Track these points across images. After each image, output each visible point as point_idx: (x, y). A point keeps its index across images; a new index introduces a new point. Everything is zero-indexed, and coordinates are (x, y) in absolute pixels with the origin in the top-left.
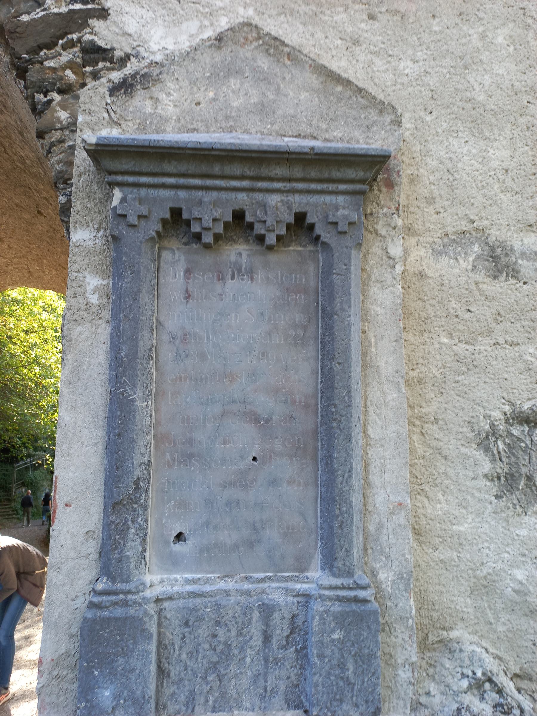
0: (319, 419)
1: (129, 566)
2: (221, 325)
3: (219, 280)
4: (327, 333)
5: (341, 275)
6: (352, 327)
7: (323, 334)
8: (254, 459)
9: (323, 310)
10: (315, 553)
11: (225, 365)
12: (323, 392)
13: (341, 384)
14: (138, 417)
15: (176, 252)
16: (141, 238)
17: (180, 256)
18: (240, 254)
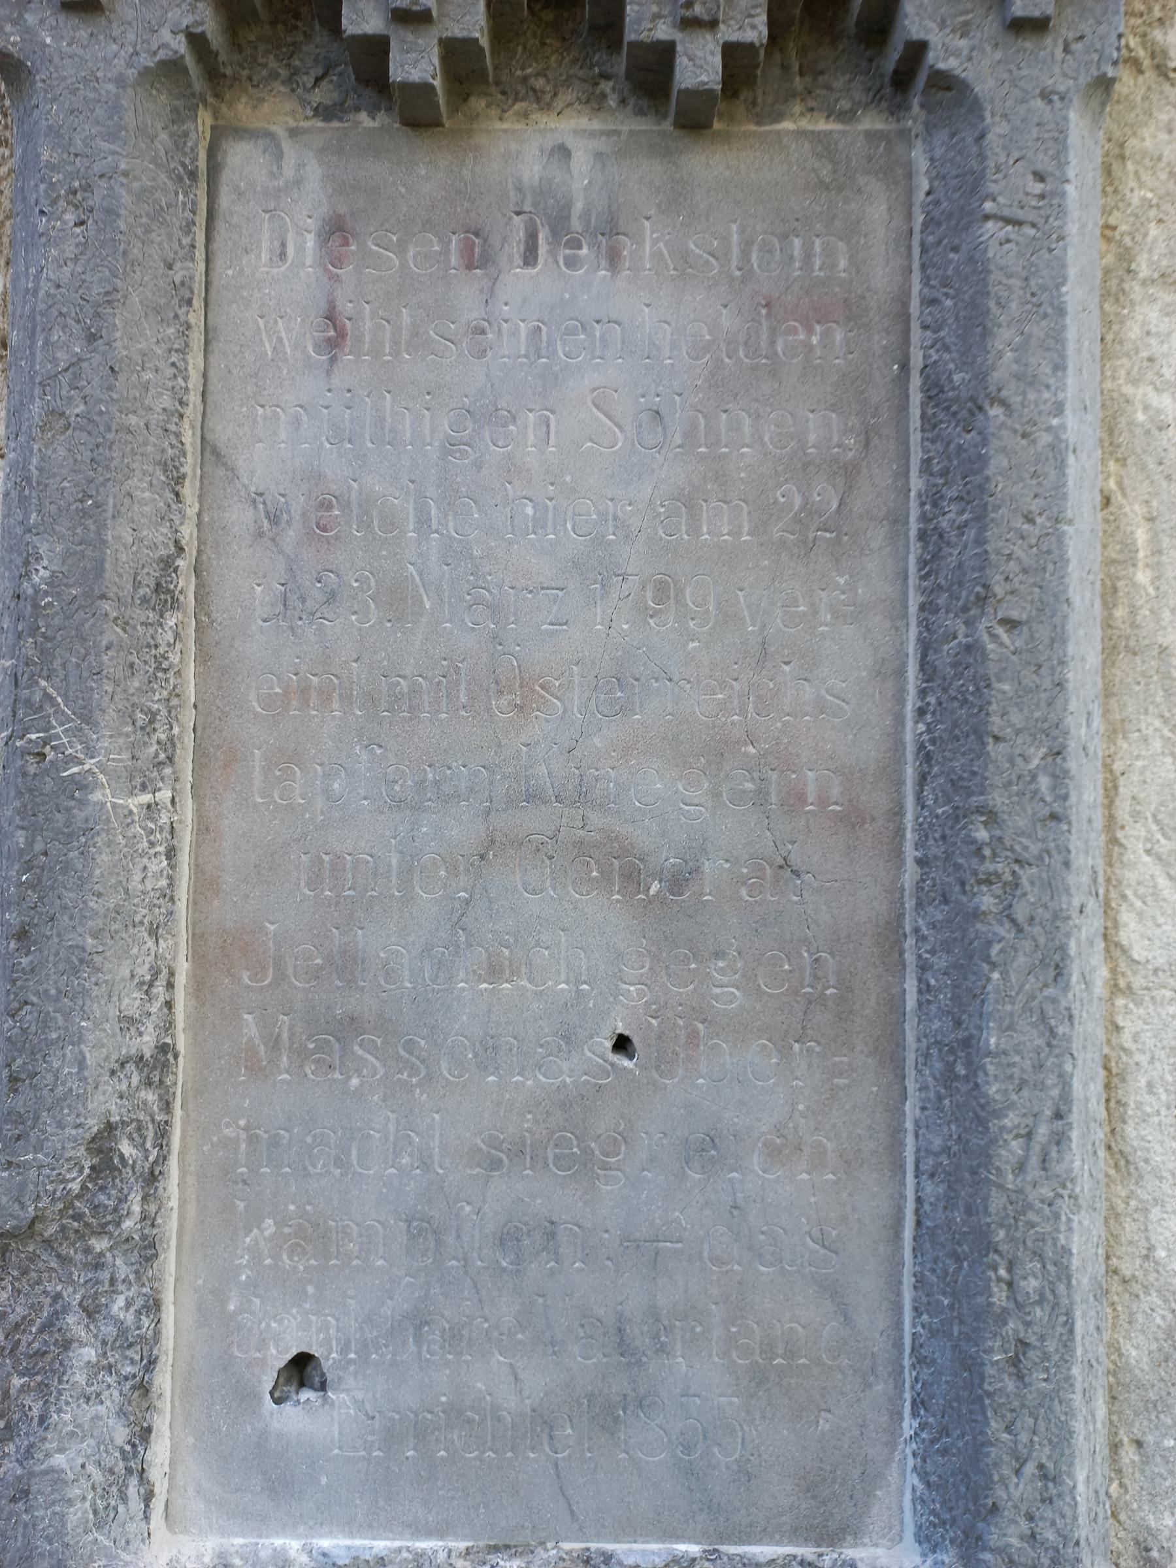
0: (910, 874)
1: (62, 1518)
2: (478, 465)
3: (470, 266)
4: (952, 492)
5: (1018, 223)
6: (1071, 459)
7: (933, 499)
8: (622, 1044)
9: (934, 390)
10: (888, 1462)
11: (496, 639)
12: (928, 757)
13: (1016, 718)
14: (104, 858)
15: (286, 145)
16: (120, 63)
17: (300, 166)
18: (563, 152)
